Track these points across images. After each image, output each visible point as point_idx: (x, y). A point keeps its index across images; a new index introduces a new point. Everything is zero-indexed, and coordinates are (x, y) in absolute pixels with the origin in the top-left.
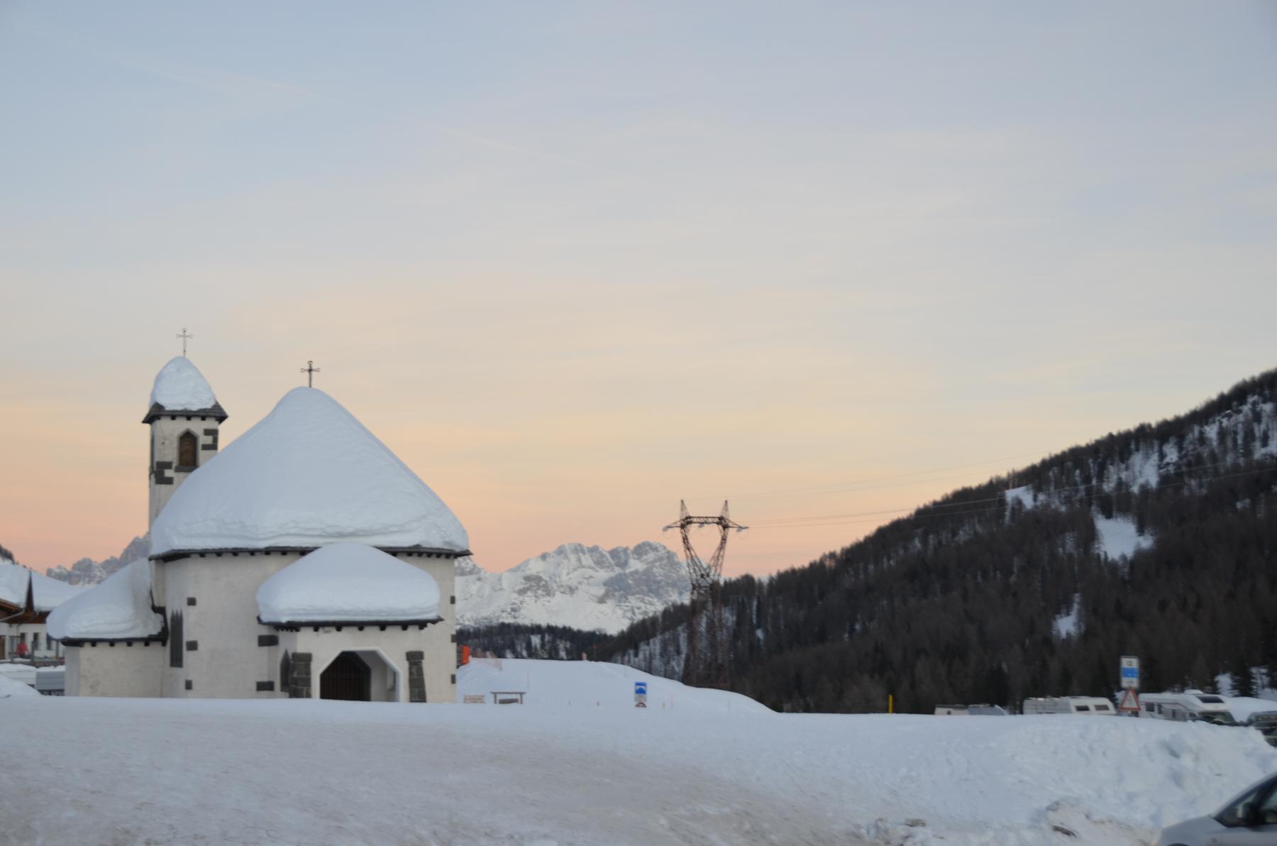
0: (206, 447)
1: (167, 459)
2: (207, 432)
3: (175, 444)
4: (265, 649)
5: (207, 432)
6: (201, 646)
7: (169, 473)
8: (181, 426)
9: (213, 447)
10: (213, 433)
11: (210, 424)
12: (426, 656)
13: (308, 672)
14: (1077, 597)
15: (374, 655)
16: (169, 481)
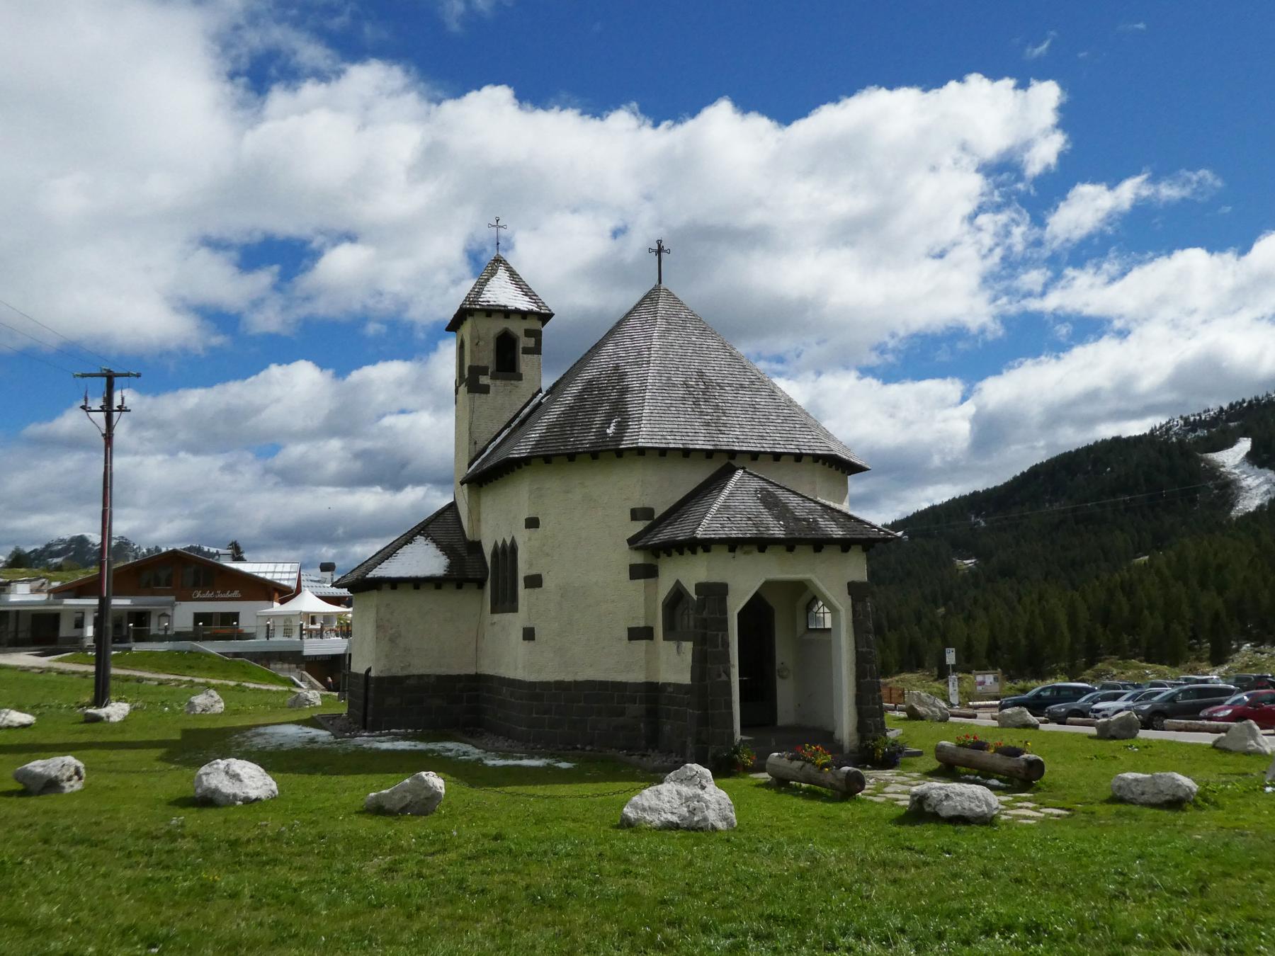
0: (527, 351)
1: (481, 364)
2: (529, 333)
3: (492, 346)
4: (641, 582)
5: (529, 333)
6: (547, 582)
7: (484, 380)
8: (498, 325)
9: (537, 350)
10: (537, 335)
11: (533, 324)
12: (850, 580)
13: (724, 611)
14: (695, 597)
15: (810, 581)
16: (485, 390)
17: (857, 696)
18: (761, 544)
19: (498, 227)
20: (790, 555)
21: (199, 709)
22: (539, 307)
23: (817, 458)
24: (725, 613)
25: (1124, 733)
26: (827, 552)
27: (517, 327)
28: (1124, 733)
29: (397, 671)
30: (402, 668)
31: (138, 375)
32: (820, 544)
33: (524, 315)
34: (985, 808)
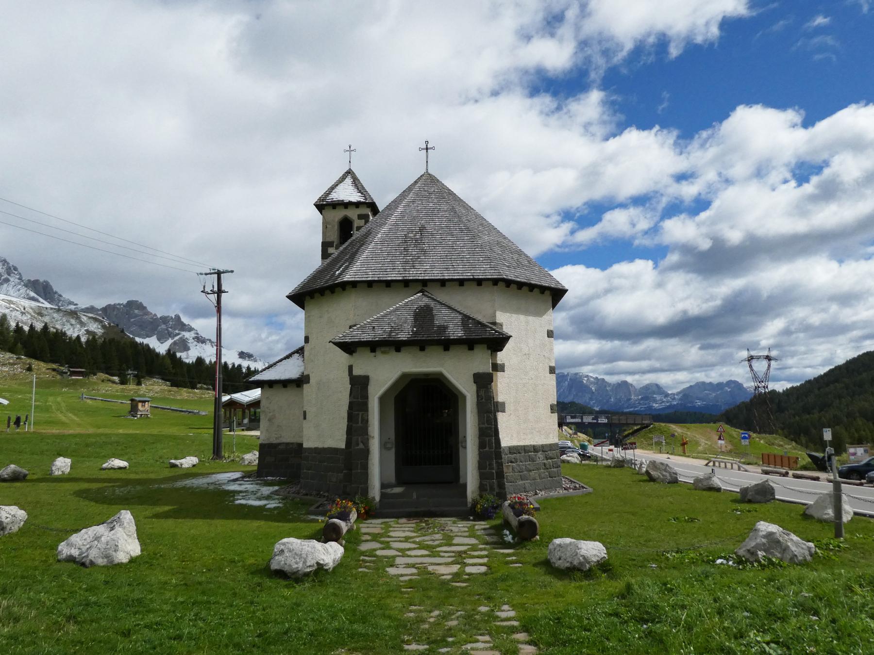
2: (360, 217)
3: (336, 227)
5: (360, 217)
8: (340, 214)
17: (479, 462)
18: (398, 346)
19: (350, 151)
20: (422, 353)
21: (247, 462)
22: (366, 199)
23: (495, 282)
24: (367, 398)
25: (759, 498)
26: (454, 351)
27: (352, 214)
28: (759, 498)
29: (274, 441)
30: (276, 438)
31: (232, 272)
32: (447, 344)
33: (357, 205)
34: (301, 565)
